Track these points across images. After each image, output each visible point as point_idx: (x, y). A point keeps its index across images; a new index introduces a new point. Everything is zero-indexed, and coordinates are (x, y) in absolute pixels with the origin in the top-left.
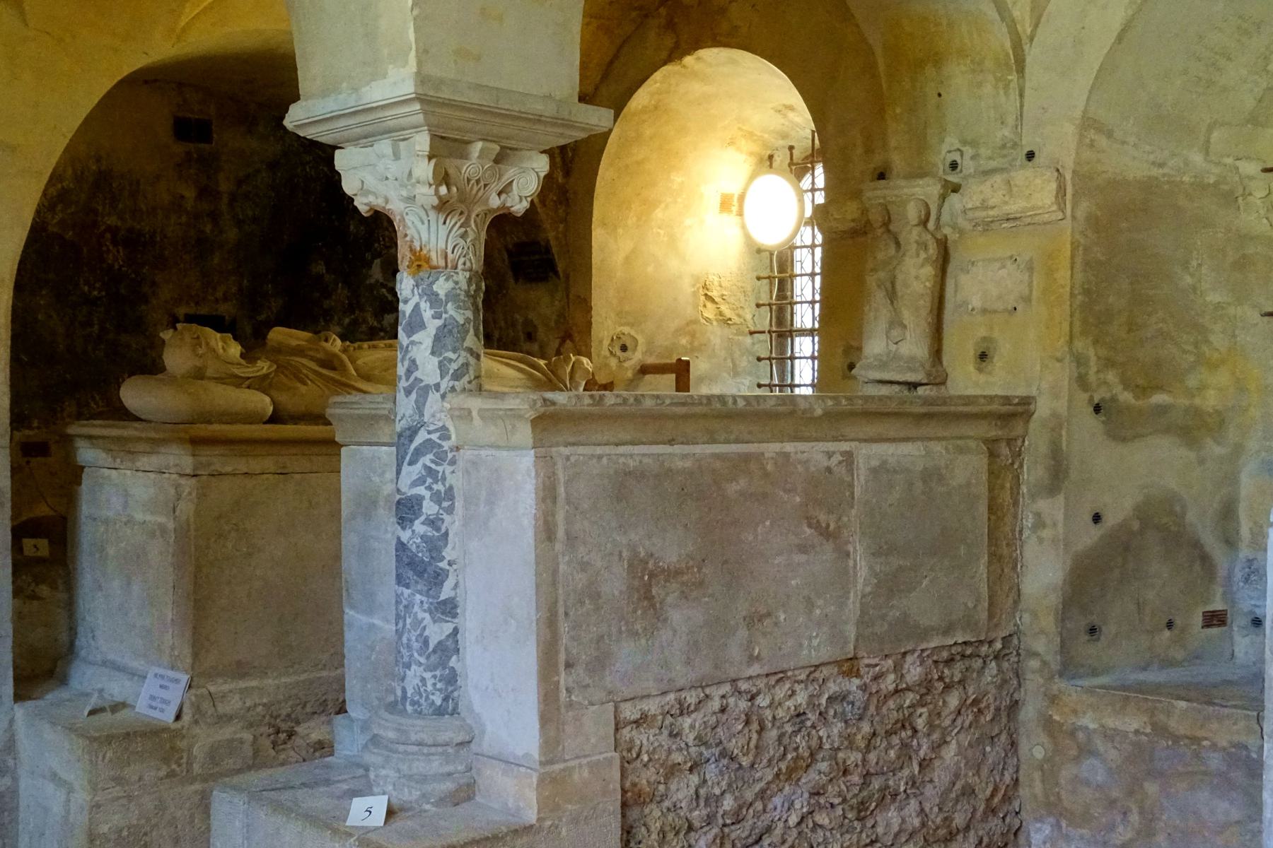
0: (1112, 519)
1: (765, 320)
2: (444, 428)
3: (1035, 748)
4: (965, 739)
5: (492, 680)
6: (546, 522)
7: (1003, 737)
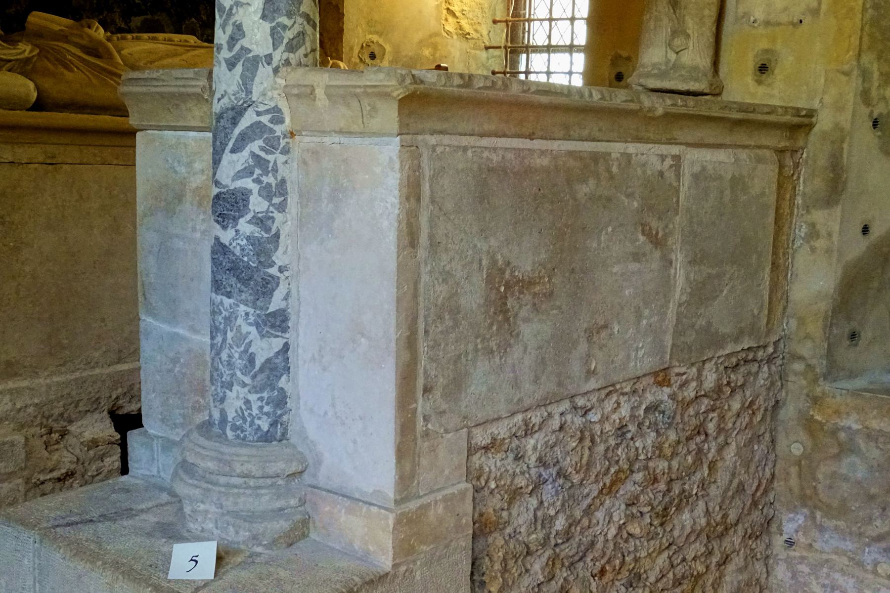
0: (877, 231)
1: (500, 36)
2: (276, 110)
3: (794, 445)
4: (742, 439)
5: (333, 405)
6: (409, 225)
7: (767, 435)
